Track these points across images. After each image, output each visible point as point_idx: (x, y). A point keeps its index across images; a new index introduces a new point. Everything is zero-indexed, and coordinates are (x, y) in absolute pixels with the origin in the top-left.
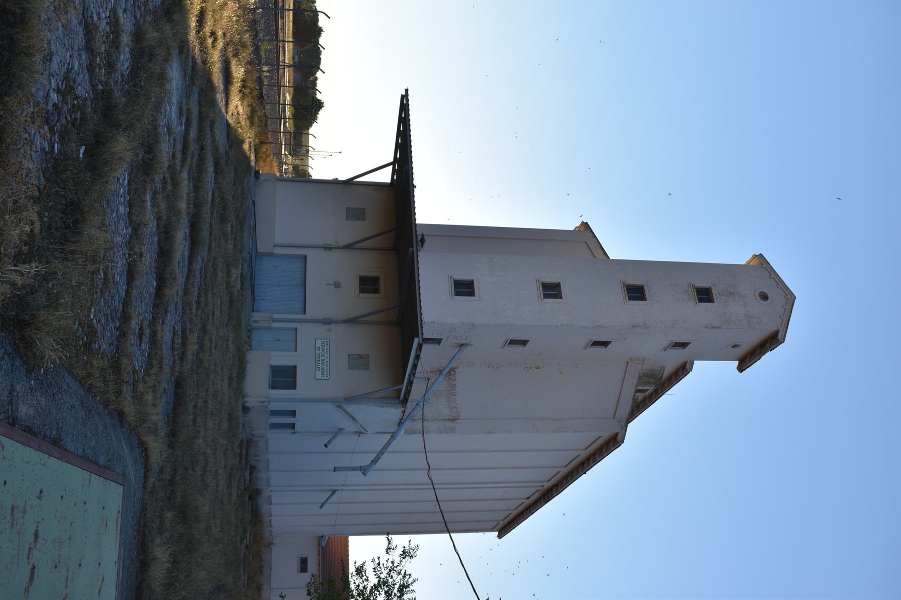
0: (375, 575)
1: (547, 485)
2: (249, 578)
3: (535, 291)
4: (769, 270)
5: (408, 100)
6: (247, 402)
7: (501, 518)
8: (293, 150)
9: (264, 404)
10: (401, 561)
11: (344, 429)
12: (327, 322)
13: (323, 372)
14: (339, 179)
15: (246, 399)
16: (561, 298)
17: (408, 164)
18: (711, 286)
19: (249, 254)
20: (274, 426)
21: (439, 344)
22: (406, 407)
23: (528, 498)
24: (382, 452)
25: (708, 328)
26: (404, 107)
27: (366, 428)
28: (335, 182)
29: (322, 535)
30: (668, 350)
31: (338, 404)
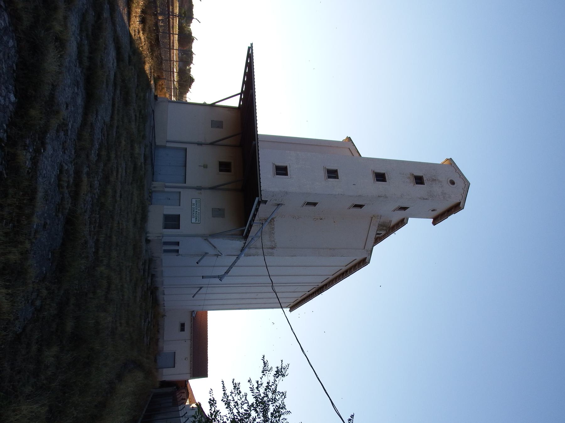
0: (253, 395)
1: (320, 285)
3: (322, 174)
4: (455, 167)
5: (252, 50)
6: (149, 236)
7: (292, 301)
8: (178, 99)
9: (159, 238)
10: (275, 381)
12: (199, 188)
14: (207, 103)
15: (148, 235)
16: (338, 178)
17: (252, 89)
18: (423, 175)
19: (150, 143)
20: (166, 251)
23: (309, 291)
24: (231, 267)
25: (421, 199)
26: (250, 56)
27: (221, 253)
28: (204, 105)
29: (193, 310)
30: (396, 211)
31: (205, 238)
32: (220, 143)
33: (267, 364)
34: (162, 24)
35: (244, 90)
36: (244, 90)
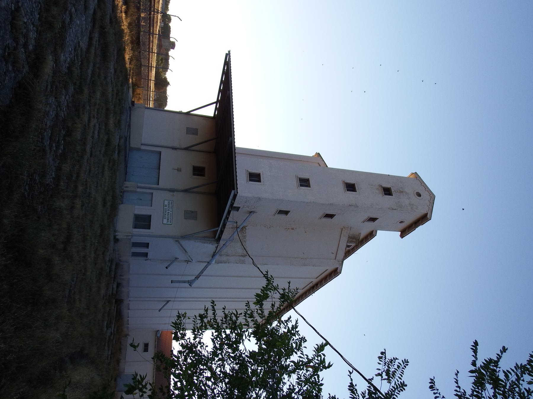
2: (112, 354)
3: (295, 183)
5: (230, 59)
11: (178, 258)
12: (172, 190)
13: (168, 220)
14: (183, 111)
16: (310, 187)
19: (125, 137)
20: (135, 254)
21: (238, 211)
22: (219, 243)
25: (390, 209)
26: (227, 64)
28: (180, 113)
30: (365, 222)
31: (176, 239)
32: (194, 148)
33: (272, 280)
34: (144, 24)
35: (222, 88)
36: (222, 88)
